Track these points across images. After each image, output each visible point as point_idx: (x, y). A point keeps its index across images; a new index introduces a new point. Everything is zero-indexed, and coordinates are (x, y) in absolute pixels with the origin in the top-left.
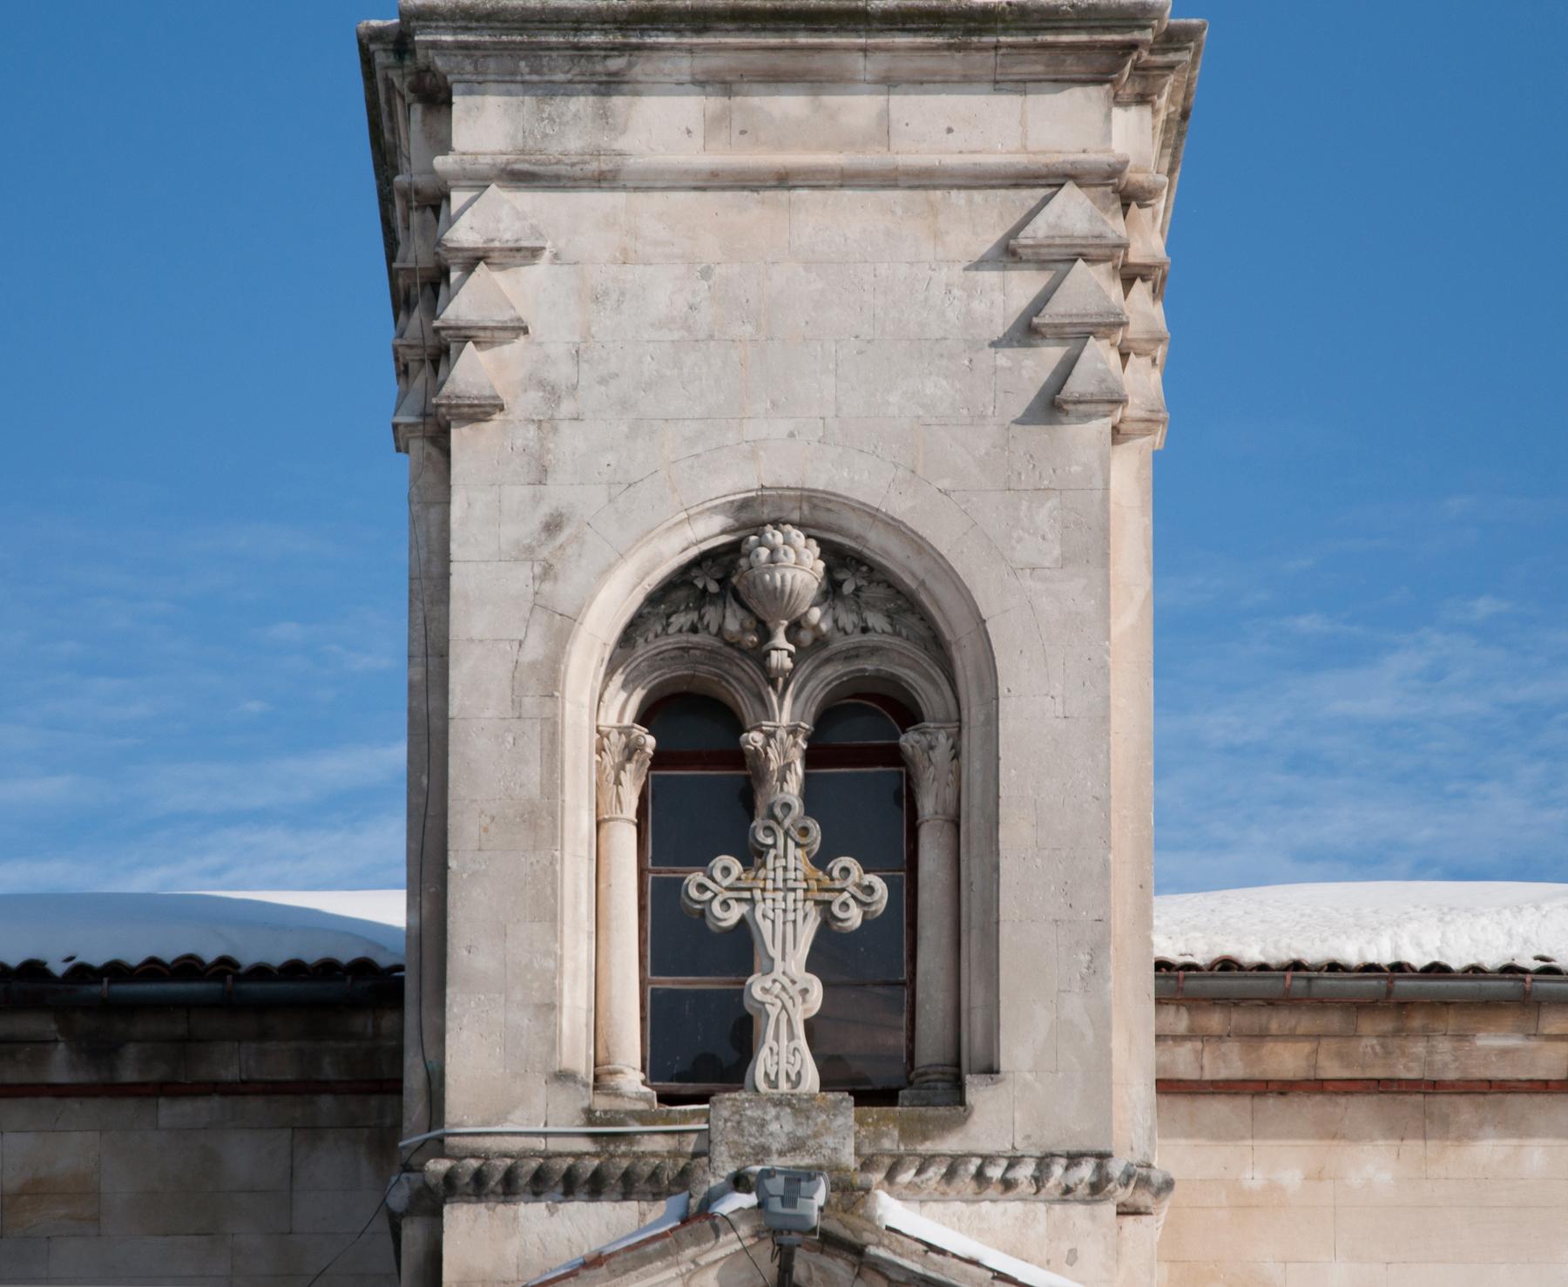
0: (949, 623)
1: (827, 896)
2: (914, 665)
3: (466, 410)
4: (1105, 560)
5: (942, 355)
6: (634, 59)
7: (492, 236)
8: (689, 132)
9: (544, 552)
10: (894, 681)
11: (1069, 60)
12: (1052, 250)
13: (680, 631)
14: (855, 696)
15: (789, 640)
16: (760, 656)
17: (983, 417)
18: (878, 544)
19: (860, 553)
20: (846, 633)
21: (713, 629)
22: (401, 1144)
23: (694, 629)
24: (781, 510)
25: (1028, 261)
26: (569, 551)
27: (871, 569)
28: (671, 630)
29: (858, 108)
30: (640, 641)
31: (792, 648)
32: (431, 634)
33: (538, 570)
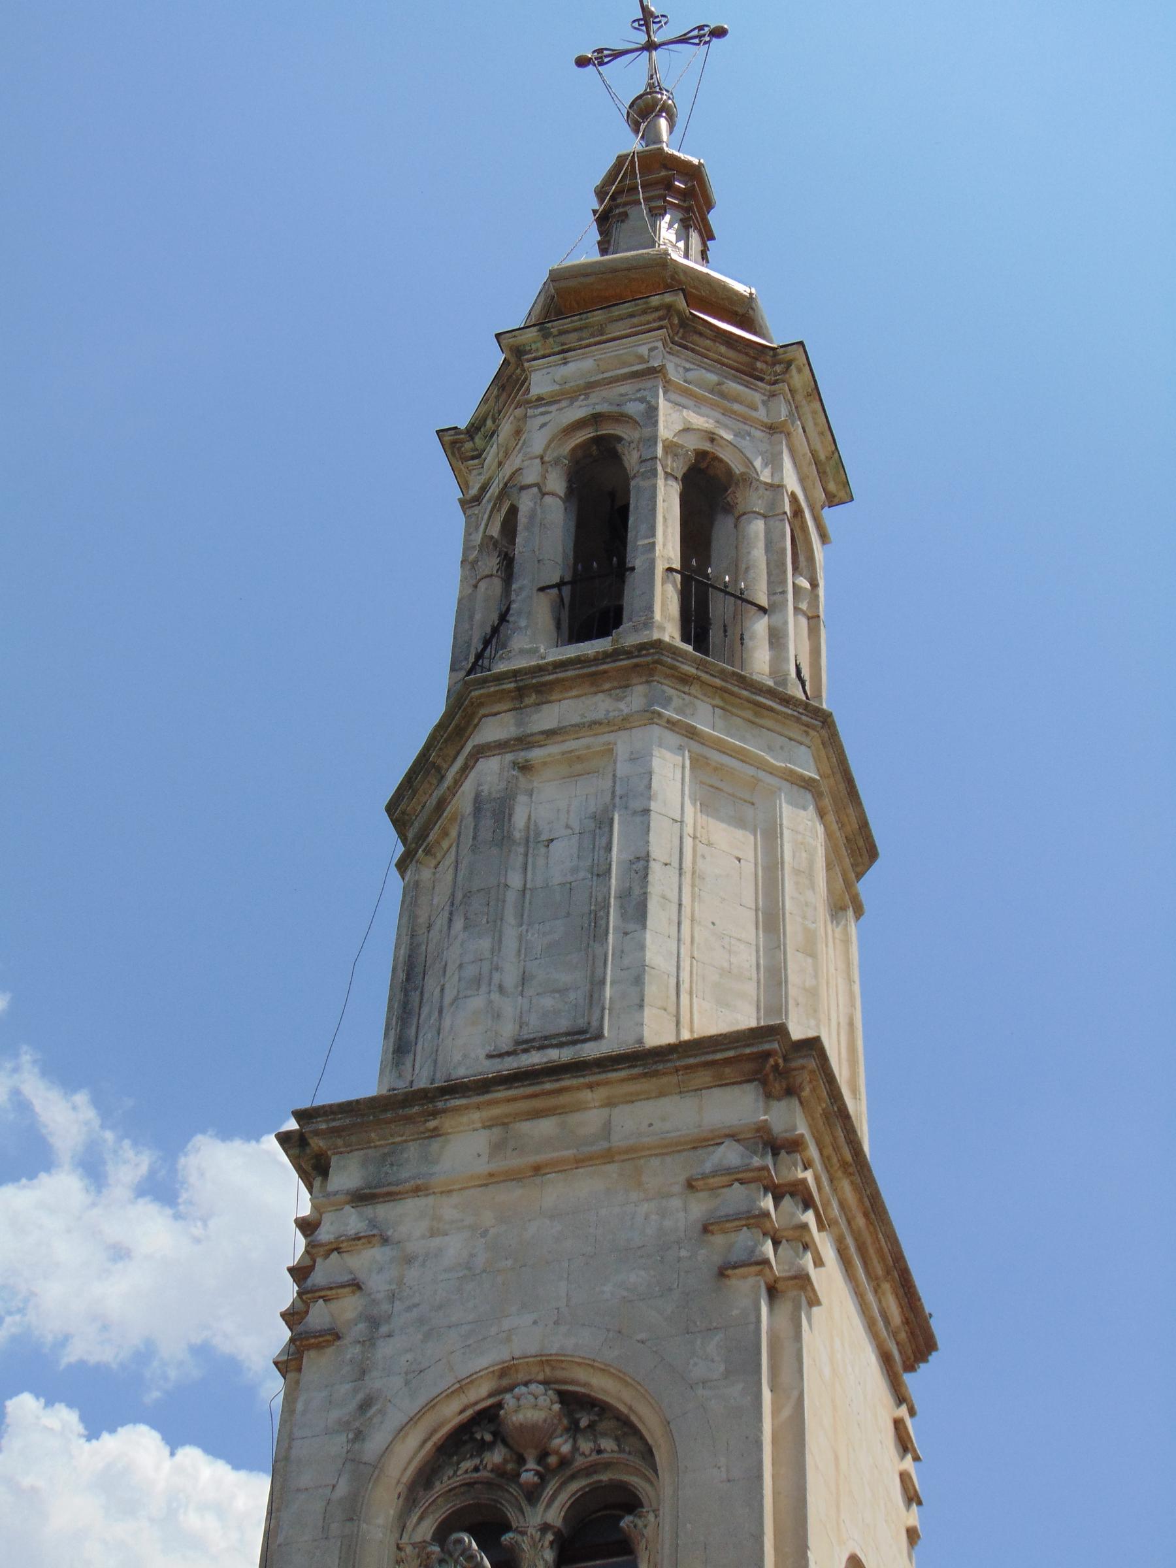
0: (649, 1430)
9: (357, 1424)
11: (727, 1070)
13: (466, 1472)
17: (670, 1289)
25: (702, 1190)
26: (375, 1420)
28: (459, 1473)
30: (437, 1483)
33: (351, 1436)
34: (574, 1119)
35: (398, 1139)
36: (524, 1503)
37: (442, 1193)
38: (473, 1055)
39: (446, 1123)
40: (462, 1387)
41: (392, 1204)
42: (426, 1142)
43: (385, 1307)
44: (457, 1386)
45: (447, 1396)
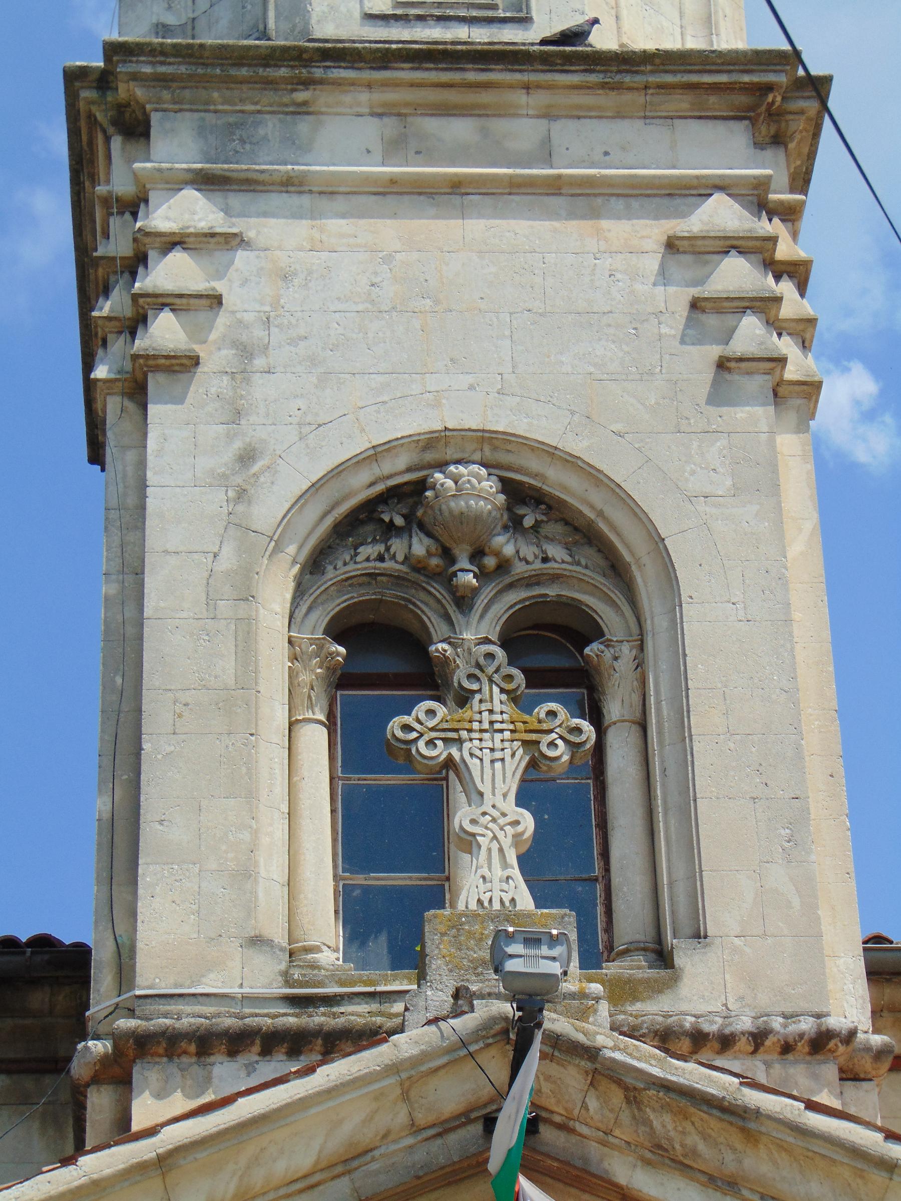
1: (534, 737)
2: (595, 590)
3: (163, 361)
4: (775, 489)
5: (610, 325)
6: (317, 92)
7: (189, 224)
8: (369, 152)
9: (238, 480)
10: (574, 607)
11: (712, 99)
12: (706, 242)
13: (368, 559)
14: (535, 627)
15: (471, 563)
16: (447, 578)
18: (557, 481)
19: (538, 490)
20: (528, 563)
21: (400, 557)
22: (87, 1014)
23: (381, 558)
24: (463, 451)
25: (685, 252)
26: (262, 479)
27: (550, 507)
28: (358, 559)
29: (524, 132)
30: (330, 568)
31: (476, 570)
32: (126, 555)
34: (499, 126)
35: (250, 107)
36: (452, 610)
37: (321, 193)
38: (343, 9)
39: (322, 98)
40: (376, 454)
41: (250, 195)
42: (289, 118)
43: (259, 333)
44: (372, 452)
45: (358, 462)
